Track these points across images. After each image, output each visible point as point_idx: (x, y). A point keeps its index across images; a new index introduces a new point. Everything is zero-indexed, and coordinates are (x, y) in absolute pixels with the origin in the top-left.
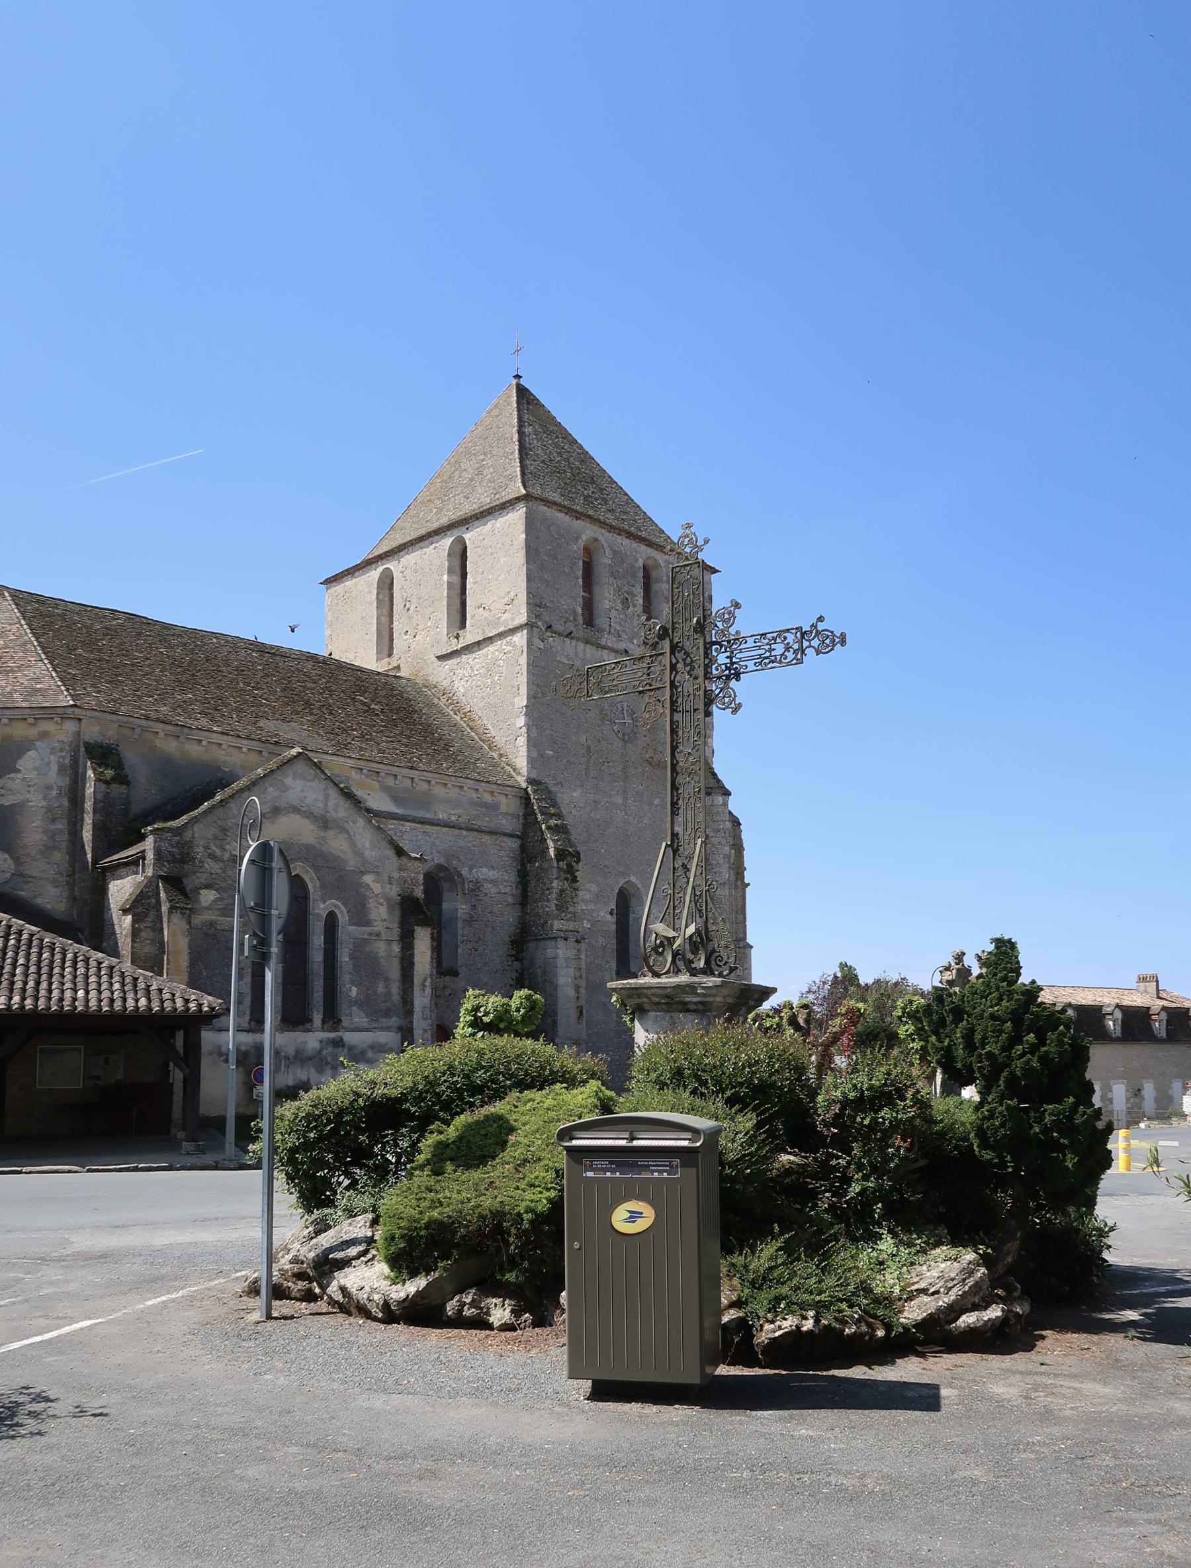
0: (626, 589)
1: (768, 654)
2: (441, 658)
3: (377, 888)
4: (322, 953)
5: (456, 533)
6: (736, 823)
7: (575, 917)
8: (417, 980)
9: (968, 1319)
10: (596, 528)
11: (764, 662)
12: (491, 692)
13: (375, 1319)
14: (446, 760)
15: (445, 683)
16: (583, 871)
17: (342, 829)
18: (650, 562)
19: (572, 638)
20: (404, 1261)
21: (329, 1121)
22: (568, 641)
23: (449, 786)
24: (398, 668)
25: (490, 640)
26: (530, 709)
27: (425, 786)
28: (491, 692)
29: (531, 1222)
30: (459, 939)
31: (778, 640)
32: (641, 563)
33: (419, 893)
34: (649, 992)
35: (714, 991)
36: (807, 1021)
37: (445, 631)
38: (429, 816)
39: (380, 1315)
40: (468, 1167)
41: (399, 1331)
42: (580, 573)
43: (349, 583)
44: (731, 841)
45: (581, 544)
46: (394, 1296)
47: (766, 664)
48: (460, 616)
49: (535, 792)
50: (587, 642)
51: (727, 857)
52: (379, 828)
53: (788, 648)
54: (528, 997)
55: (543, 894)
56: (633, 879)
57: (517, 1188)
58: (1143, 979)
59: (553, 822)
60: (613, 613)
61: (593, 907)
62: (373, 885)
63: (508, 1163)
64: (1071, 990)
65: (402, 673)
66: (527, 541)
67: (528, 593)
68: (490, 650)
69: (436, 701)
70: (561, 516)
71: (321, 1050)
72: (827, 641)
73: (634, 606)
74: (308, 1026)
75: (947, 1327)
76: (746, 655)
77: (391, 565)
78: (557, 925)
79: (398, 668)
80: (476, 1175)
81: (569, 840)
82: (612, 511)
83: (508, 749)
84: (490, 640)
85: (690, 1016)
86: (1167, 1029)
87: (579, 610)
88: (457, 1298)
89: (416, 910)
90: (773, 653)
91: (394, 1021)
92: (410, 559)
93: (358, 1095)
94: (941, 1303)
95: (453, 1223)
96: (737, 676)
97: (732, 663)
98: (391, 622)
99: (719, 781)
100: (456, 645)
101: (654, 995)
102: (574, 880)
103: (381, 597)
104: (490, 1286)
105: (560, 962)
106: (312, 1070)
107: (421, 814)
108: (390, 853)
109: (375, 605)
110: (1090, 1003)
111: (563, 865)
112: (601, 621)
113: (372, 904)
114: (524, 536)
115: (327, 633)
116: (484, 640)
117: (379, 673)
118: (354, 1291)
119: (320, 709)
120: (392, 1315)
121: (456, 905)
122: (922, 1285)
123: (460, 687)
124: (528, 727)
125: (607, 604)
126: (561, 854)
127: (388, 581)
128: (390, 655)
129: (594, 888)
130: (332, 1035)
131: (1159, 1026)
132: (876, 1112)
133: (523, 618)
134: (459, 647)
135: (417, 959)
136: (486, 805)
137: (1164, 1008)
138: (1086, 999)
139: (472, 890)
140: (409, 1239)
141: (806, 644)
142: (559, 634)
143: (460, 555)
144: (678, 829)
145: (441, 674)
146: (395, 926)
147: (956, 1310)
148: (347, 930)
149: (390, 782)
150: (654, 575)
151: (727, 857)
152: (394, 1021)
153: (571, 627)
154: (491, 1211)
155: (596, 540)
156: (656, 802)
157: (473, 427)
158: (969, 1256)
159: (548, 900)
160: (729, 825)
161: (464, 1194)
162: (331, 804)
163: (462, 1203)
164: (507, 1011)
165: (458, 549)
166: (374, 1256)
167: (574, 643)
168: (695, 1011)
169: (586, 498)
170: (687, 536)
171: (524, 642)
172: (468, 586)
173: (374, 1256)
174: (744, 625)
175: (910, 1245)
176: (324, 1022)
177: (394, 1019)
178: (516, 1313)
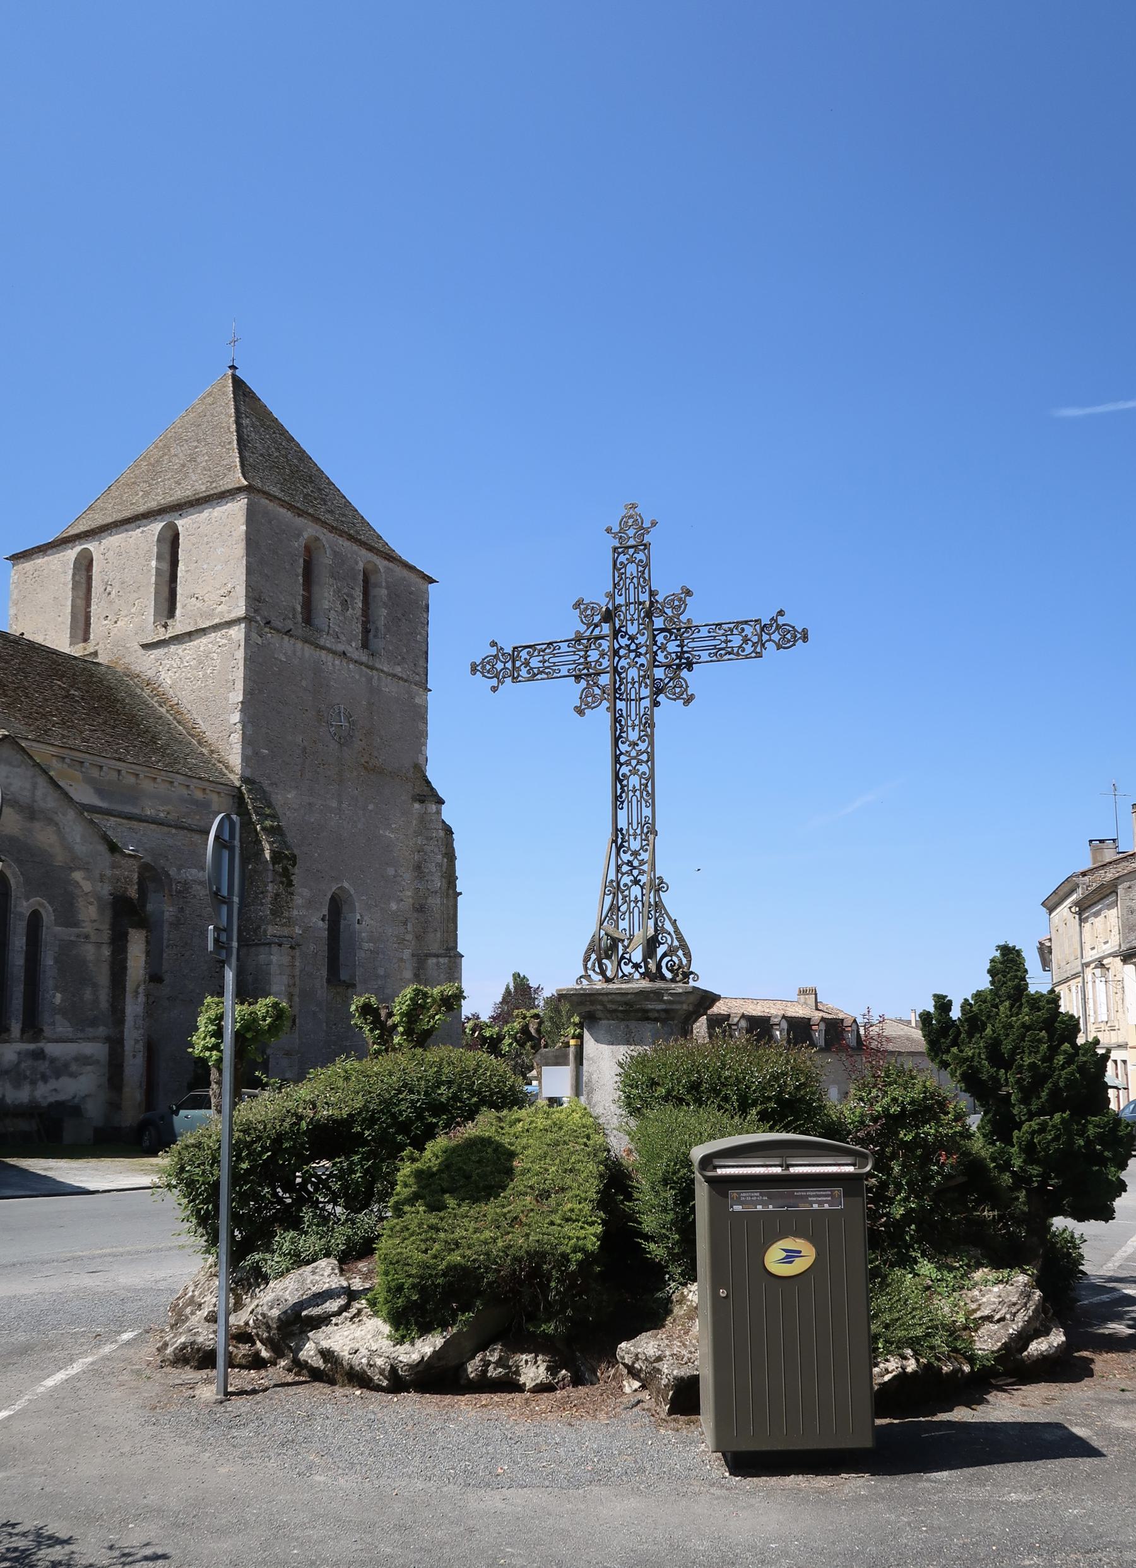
0: (345, 590)
1: (723, 645)
2: (146, 647)
3: (87, 886)
4: (23, 955)
5: (168, 518)
6: (449, 831)
7: (290, 922)
8: (130, 986)
9: (1038, 1347)
10: (317, 527)
11: (720, 653)
12: (204, 685)
13: (378, 1388)
14: (154, 753)
15: (150, 673)
16: (298, 875)
17: (50, 821)
18: (370, 567)
19: (291, 636)
20: (408, 1319)
21: (265, 1149)
22: (286, 638)
23: (159, 780)
24: (95, 654)
25: (203, 631)
26: (248, 706)
27: (132, 780)
28: (204, 685)
29: (580, 1263)
30: (165, 942)
31: (735, 632)
32: (361, 566)
33: (133, 892)
34: (605, 998)
35: (684, 998)
36: (538, 1031)
37: (152, 619)
38: (136, 811)
39: (385, 1383)
40: (476, 1200)
41: (410, 1402)
42: (300, 571)
43: (40, 561)
44: (443, 849)
45: (302, 541)
46: (404, 1358)
48: (168, 603)
49: (249, 791)
50: (306, 641)
51: (440, 865)
52: (91, 821)
53: (746, 640)
54: (275, 1005)
55: (257, 897)
56: (346, 885)
57: (552, 1223)
58: (803, 992)
59: (268, 823)
60: (332, 614)
61: (308, 915)
62: (83, 883)
63: (525, 1194)
64: (742, 1002)
65: (99, 660)
66: (247, 533)
67: (247, 586)
68: (202, 642)
69: (138, 691)
70: (283, 511)
71: (19, 1063)
72: (789, 636)
73: (353, 609)
74: (5, 1036)
75: (1019, 1357)
76: (567, 659)
77: (91, 546)
78: (271, 930)
79: (95, 654)
80: (490, 1209)
81: (285, 842)
82: (331, 512)
83: (221, 746)
84: (203, 631)
85: (649, 1026)
87: (299, 609)
88: (479, 1357)
89: (126, 913)
90: (729, 645)
91: (102, 1031)
92: (113, 541)
93: (301, 1118)
94: (1011, 1331)
95: (479, 1267)
96: (689, 666)
97: (683, 652)
98: (88, 605)
100: (163, 635)
102: (290, 884)
103: (77, 578)
104: (518, 1338)
105: (274, 969)
106: (8, 1086)
107: (128, 809)
108: (102, 848)
109: (70, 586)
111: (279, 868)
112: (320, 621)
113: (81, 903)
114: (244, 528)
115: (12, 611)
116: (197, 631)
117: (75, 658)
118: (345, 1354)
119: (14, 691)
120: (398, 1382)
121: (164, 908)
122: (986, 1312)
123: (167, 679)
124: (244, 723)
125: (326, 605)
126: (277, 857)
127: (85, 562)
128: (86, 639)
129: (306, 892)
130: (32, 1046)
131: (818, 1035)
132: (918, 1128)
133: (241, 611)
134: (167, 636)
135: (130, 964)
136: (196, 802)
137: (823, 1019)
138: (756, 1010)
139: (180, 892)
140: (422, 1289)
141: (765, 637)
142: (278, 631)
143: (171, 543)
144: (622, 823)
145: (146, 664)
146: (106, 927)
147: (1024, 1338)
148: (53, 931)
149: (95, 773)
150: (373, 579)
151: (440, 865)
152: (102, 1031)
153: (289, 624)
154: (527, 1252)
155: (317, 539)
156: (371, 807)
157: (183, 413)
158: (1022, 1279)
159: (262, 904)
160: (442, 833)
161: (477, 1233)
162: (39, 793)
163: (486, 1243)
164: (255, 1020)
165: (169, 534)
166: (359, 1312)
167: (292, 641)
169: (306, 496)
170: (631, 517)
171: (242, 636)
172: (179, 574)
173: (359, 1312)
174: (695, 613)
175: (951, 1269)
176: (23, 1031)
177: (101, 1029)
178: (552, 1370)
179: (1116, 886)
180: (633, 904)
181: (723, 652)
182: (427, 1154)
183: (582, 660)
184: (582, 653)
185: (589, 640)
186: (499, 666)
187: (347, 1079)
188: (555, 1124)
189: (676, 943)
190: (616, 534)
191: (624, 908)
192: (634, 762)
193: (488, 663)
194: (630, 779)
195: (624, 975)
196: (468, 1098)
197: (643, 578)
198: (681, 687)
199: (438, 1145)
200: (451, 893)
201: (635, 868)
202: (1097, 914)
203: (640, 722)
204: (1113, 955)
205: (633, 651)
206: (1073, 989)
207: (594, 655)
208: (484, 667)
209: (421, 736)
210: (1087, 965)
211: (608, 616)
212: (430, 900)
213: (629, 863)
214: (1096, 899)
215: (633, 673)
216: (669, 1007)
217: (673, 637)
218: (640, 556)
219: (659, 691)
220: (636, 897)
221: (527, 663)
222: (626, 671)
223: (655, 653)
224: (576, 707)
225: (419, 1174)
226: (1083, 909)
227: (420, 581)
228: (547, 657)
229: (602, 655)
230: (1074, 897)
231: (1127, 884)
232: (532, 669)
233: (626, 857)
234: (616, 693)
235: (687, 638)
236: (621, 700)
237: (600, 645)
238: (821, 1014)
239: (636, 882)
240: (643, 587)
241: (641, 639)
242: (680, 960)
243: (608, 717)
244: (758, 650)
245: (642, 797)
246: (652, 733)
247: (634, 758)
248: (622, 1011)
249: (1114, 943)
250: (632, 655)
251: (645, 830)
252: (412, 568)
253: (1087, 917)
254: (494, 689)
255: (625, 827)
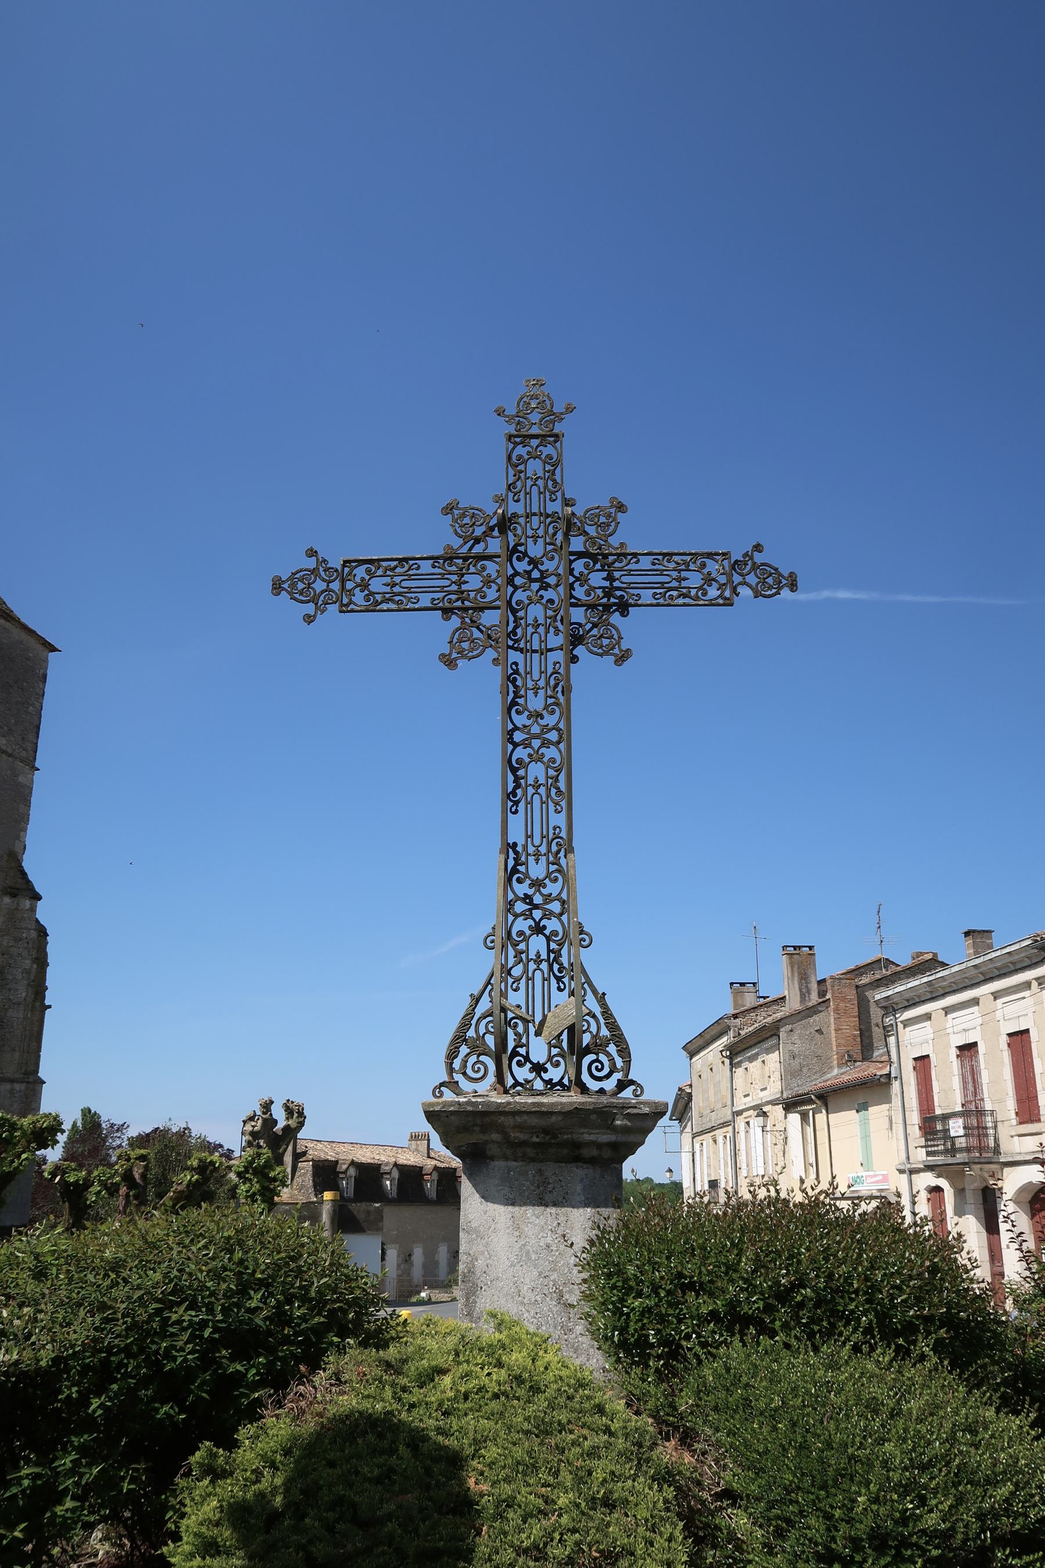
1: (675, 584)
6: (42, 933)
34: (509, 1121)
36: (143, 1176)
44: (34, 953)
47: (671, 597)
86: (437, 1190)
96: (623, 608)
97: (613, 589)
99: (28, 882)
101: (520, 1127)
110: (369, 1161)
131: (430, 1186)
137: (436, 1168)
138: (365, 1156)
141: (737, 579)
160: (34, 934)
168: (592, 1161)
179: (778, 1029)
180: (532, 966)
181: (675, 593)
182: (247, 1455)
183: (454, 587)
184: (454, 578)
185: (465, 559)
186: (319, 586)
187: (40, 1274)
188: (519, 1380)
189: (605, 1032)
190: (512, 417)
191: (517, 971)
192: (536, 743)
193: (301, 580)
194: (534, 765)
195: (517, 1083)
196: (304, 1318)
197: (552, 485)
198: (611, 637)
199: (272, 1434)
200: (37, 1006)
201: (536, 907)
202: (752, 1059)
203: (548, 683)
204: (773, 1103)
205: (535, 580)
206: (720, 1140)
207: (473, 582)
208: (293, 585)
209: (20, 821)
210: (739, 1113)
211: (505, 524)
212: (10, 1013)
213: (527, 899)
214: (751, 1043)
215: (536, 612)
216: (621, 1138)
217: (598, 566)
218: (548, 450)
219: (576, 639)
220: (538, 955)
221: (364, 585)
222: (526, 608)
223: (572, 587)
224: (443, 655)
225: (238, 1514)
226: (735, 1054)
227: (41, 648)
228: (397, 580)
229: (488, 582)
230: (724, 1040)
231: (789, 1027)
232: (372, 594)
233: (522, 889)
234: (512, 640)
235: (620, 570)
236: (516, 649)
237: (484, 568)
238: (434, 1162)
239: (538, 929)
240: (553, 493)
241: (548, 565)
242: (612, 1060)
243: (497, 675)
244: (727, 594)
245: (549, 796)
246: (568, 701)
247: (536, 737)
248: (535, 1145)
249: (775, 1089)
250: (535, 586)
251: (554, 848)
252: (32, 632)
253: (740, 1062)
254: (309, 619)
255: (521, 842)
